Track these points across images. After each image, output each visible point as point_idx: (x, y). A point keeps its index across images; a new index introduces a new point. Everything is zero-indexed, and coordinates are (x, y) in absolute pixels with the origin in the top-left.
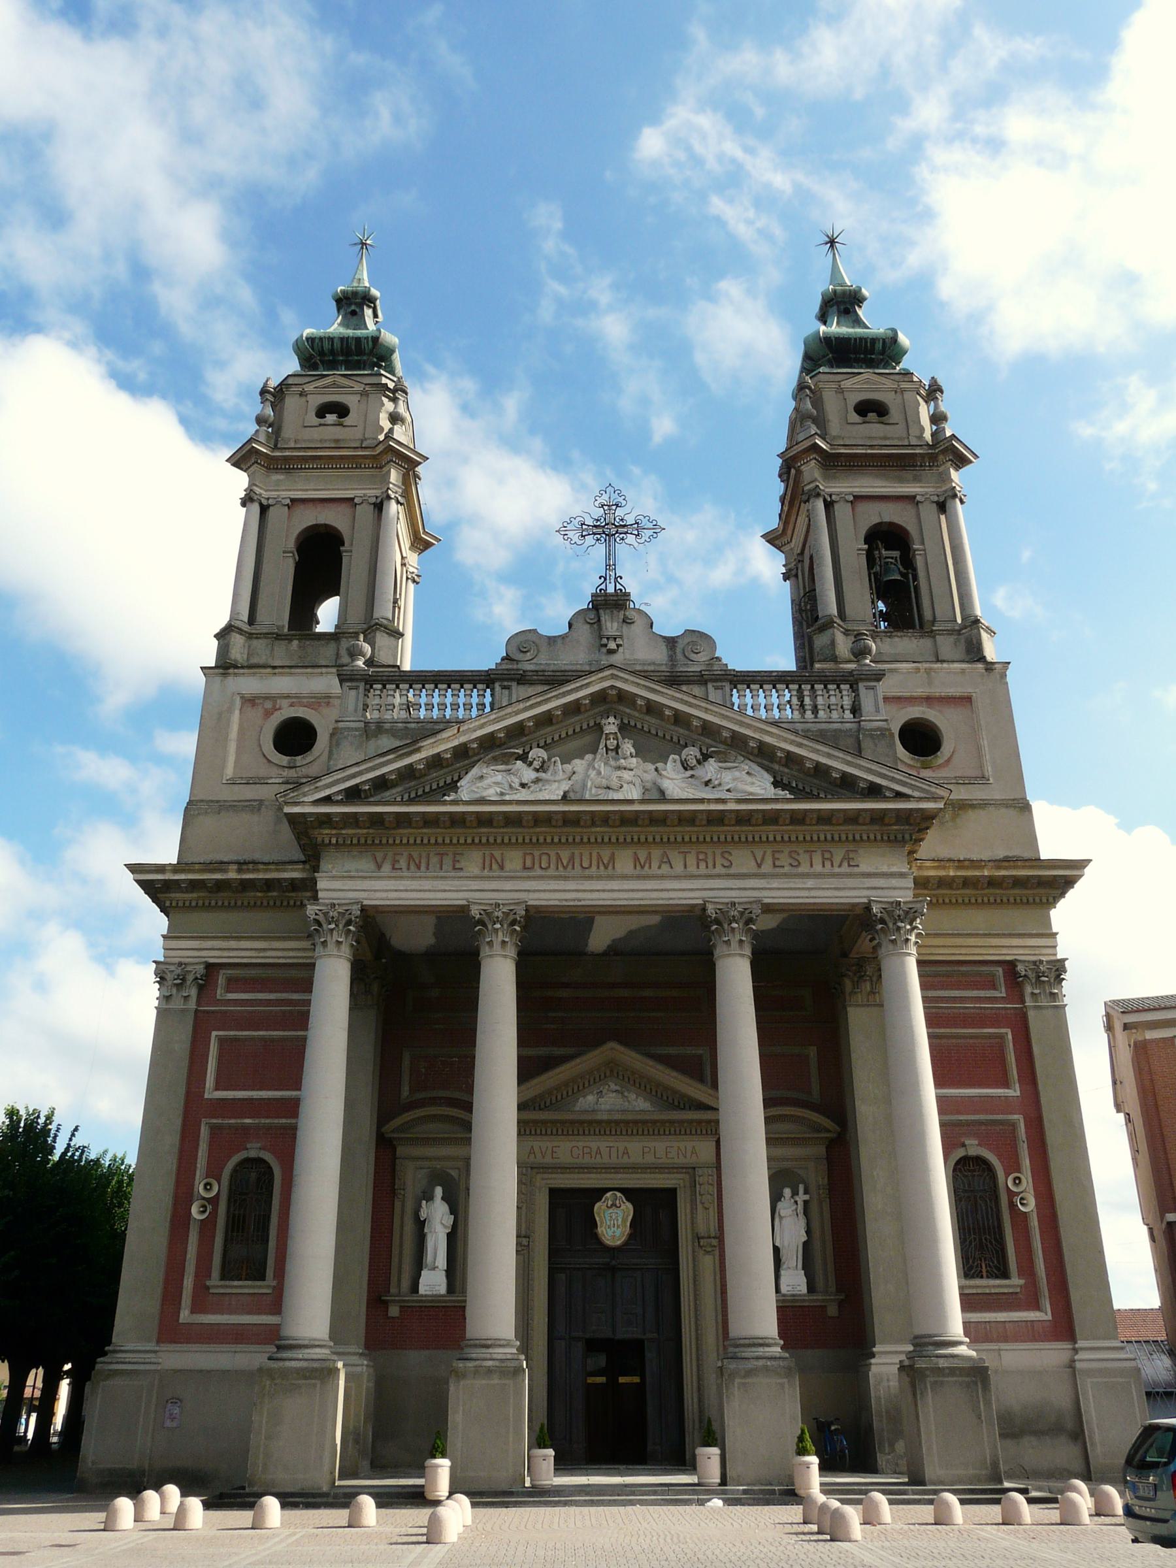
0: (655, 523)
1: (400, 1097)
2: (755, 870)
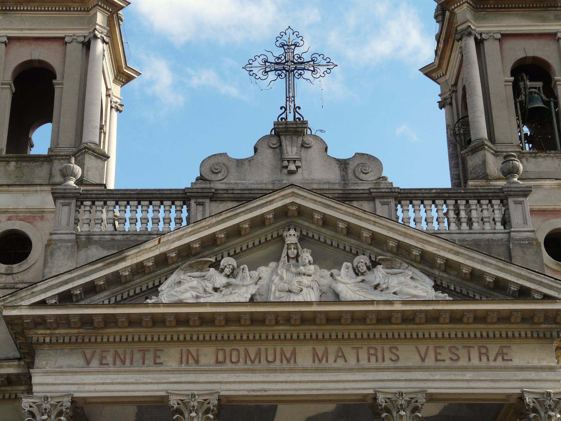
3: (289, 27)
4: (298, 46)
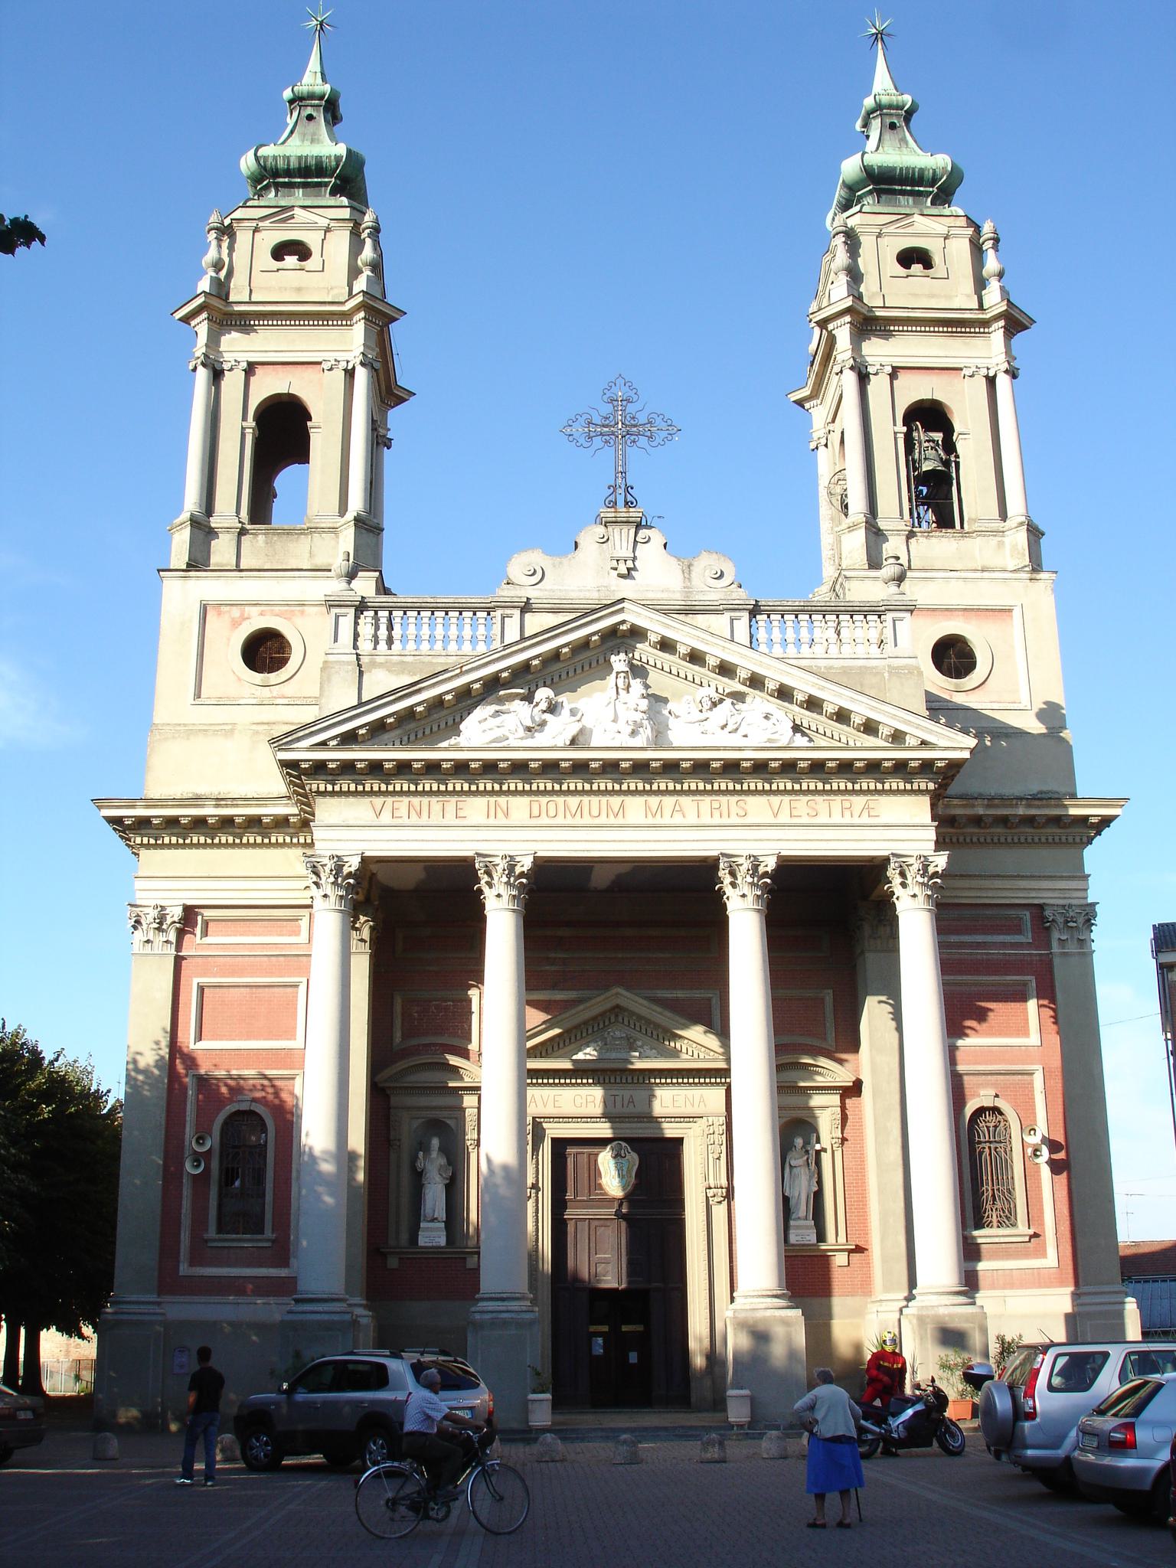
0: (669, 422)
1: (392, 1044)
2: (772, 821)
3: (620, 375)
4: (632, 402)
